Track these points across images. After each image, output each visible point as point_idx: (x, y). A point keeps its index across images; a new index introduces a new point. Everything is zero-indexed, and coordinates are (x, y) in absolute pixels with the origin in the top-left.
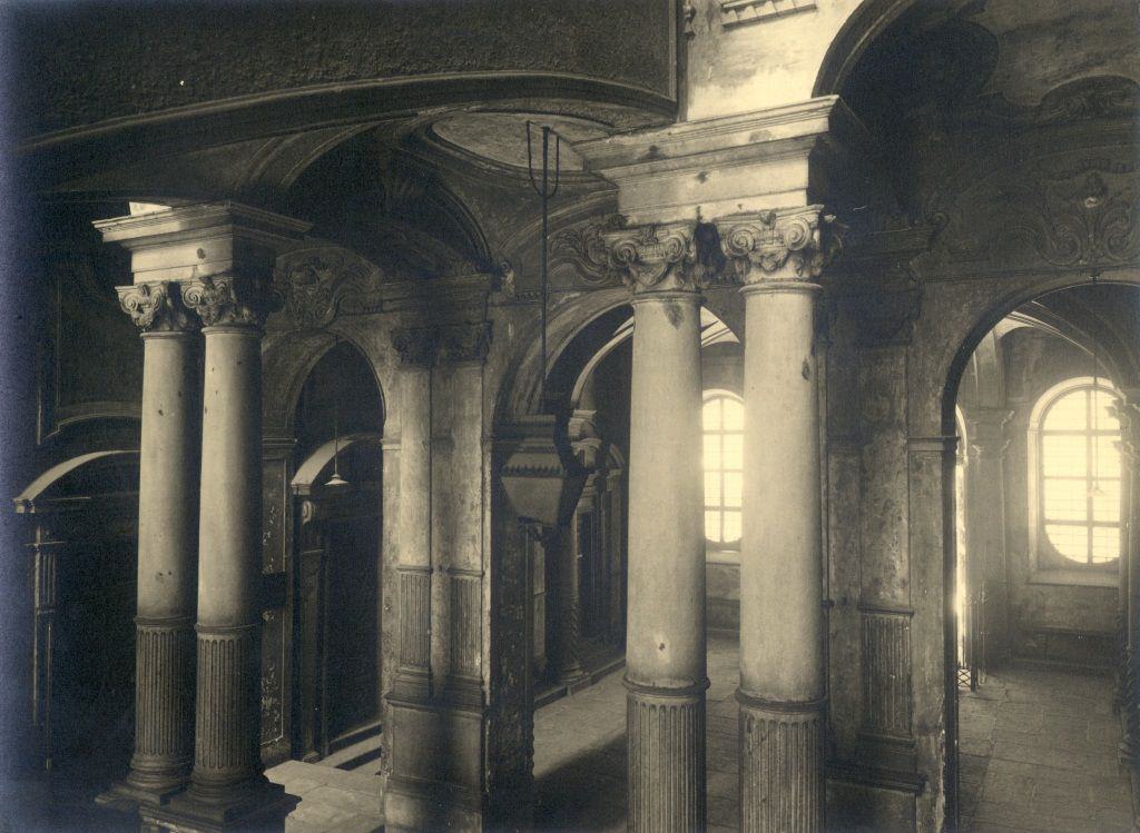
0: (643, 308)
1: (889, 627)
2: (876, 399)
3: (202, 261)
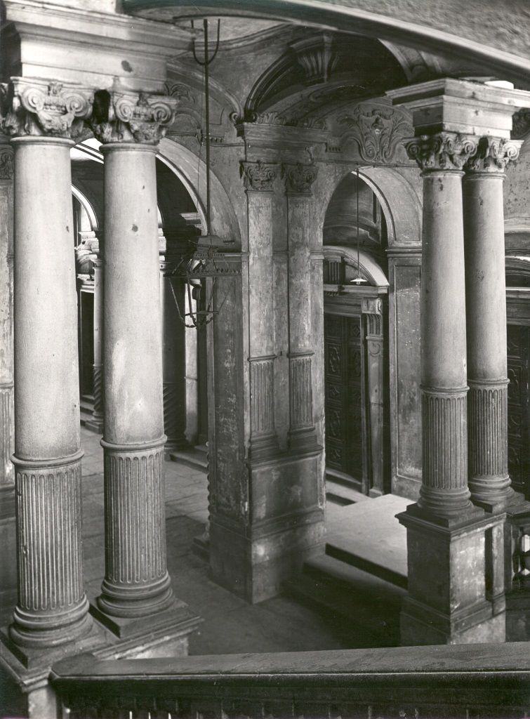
0: (452, 178)
1: (301, 365)
3: (127, 73)
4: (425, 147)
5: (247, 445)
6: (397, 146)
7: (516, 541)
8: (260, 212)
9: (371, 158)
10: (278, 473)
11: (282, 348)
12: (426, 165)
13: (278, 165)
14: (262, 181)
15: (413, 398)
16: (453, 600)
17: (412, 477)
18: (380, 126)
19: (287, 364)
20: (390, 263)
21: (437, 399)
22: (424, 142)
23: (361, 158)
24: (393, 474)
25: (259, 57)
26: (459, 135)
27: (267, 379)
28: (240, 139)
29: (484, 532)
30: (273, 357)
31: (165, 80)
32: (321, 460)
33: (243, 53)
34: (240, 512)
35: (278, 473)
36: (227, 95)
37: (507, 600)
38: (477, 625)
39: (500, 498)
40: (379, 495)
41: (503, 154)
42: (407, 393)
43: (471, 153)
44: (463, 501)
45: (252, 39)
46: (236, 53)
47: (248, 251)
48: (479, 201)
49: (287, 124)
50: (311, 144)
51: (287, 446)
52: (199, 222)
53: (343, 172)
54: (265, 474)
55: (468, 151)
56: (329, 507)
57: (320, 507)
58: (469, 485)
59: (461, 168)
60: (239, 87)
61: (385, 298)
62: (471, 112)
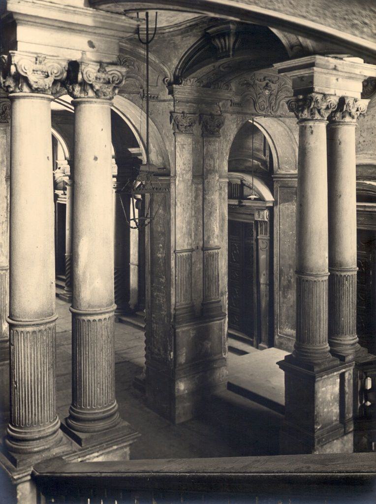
1: (212, 256)
3: (91, 49)
4: (301, 103)
5: (172, 311)
6: (281, 103)
8: (184, 148)
9: (263, 110)
11: (198, 243)
12: (301, 116)
13: (197, 115)
14: (186, 126)
19: (202, 254)
20: (275, 185)
23: (255, 110)
24: (275, 334)
25: (184, 39)
26: (325, 95)
27: (188, 266)
28: (170, 97)
30: (192, 250)
32: (225, 323)
33: (173, 35)
34: (167, 359)
35: (194, 332)
36: (161, 65)
38: (333, 440)
39: (350, 351)
40: (265, 348)
41: (355, 109)
42: (286, 277)
43: (333, 108)
44: (325, 353)
45: (180, 26)
46: (168, 36)
47: (175, 175)
50: (221, 100)
51: (202, 313)
52: (140, 154)
53: (243, 120)
54: (185, 332)
56: (230, 357)
57: (224, 356)
58: (329, 342)
59: (326, 119)
60: (170, 60)
61: (271, 209)
62: (333, 79)
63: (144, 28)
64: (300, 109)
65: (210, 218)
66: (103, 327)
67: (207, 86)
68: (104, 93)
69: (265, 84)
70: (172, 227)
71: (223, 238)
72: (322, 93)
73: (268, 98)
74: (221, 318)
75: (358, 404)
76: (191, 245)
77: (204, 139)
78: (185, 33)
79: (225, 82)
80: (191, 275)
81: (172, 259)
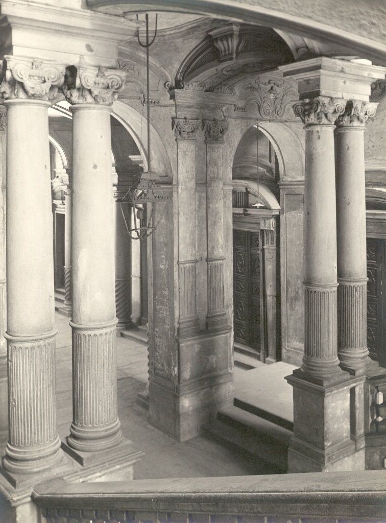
2: (213, 167)
3: (89, 53)
4: (307, 107)
5: (176, 325)
6: (287, 106)
7: (373, 396)
9: (268, 115)
10: (199, 346)
13: (200, 120)
15: (298, 291)
16: (327, 439)
17: (298, 350)
18: (274, 92)
19: (206, 265)
20: (282, 193)
21: (315, 292)
22: (307, 104)
25: (186, 41)
26: (332, 98)
27: (192, 278)
28: (172, 102)
29: (349, 390)
30: (196, 261)
31: (117, 58)
32: (230, 337)
33: (174, 38)
35: (199, 346)
36: (162, 69)
37: (366, 439)
38: (345, 457)
39: (361, 365)
41: (364, 113)
42: (293, 288)
43: (340, 112)
45: (181, 28)
48: (347, 147)
49: (206, 91)
51: (206, 327)
52: (142, 162)
53: (247, 126)
55: (338, 111)
56: (237, 371)
57: (230, 371)
58: (339, 356)
59: (333, 123)
61: (278, 218)
62: (340, 82)
63: (144, 31)
64: (306, 113)
65: (214, 228)
66: (104, 342)
67: (210, 90)
68: (103, 98)
69: (270, 88)
70: (174, 236)
71: (227, 249)
72: (329, 97)
73: (273, 102)
74: (227, 331)
75: (369, 420)
76: (195, 255)
77: (208, 146)
78: (186, 35)
79: (228, 86)
80: (195, 287)
81: (175, 271)
